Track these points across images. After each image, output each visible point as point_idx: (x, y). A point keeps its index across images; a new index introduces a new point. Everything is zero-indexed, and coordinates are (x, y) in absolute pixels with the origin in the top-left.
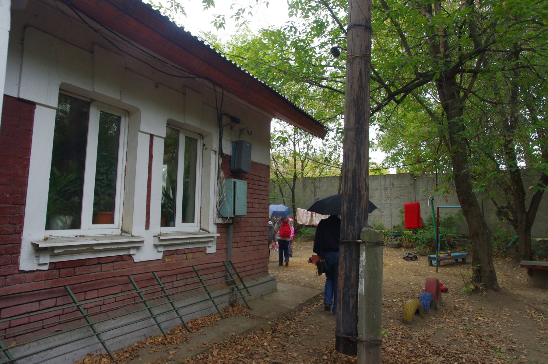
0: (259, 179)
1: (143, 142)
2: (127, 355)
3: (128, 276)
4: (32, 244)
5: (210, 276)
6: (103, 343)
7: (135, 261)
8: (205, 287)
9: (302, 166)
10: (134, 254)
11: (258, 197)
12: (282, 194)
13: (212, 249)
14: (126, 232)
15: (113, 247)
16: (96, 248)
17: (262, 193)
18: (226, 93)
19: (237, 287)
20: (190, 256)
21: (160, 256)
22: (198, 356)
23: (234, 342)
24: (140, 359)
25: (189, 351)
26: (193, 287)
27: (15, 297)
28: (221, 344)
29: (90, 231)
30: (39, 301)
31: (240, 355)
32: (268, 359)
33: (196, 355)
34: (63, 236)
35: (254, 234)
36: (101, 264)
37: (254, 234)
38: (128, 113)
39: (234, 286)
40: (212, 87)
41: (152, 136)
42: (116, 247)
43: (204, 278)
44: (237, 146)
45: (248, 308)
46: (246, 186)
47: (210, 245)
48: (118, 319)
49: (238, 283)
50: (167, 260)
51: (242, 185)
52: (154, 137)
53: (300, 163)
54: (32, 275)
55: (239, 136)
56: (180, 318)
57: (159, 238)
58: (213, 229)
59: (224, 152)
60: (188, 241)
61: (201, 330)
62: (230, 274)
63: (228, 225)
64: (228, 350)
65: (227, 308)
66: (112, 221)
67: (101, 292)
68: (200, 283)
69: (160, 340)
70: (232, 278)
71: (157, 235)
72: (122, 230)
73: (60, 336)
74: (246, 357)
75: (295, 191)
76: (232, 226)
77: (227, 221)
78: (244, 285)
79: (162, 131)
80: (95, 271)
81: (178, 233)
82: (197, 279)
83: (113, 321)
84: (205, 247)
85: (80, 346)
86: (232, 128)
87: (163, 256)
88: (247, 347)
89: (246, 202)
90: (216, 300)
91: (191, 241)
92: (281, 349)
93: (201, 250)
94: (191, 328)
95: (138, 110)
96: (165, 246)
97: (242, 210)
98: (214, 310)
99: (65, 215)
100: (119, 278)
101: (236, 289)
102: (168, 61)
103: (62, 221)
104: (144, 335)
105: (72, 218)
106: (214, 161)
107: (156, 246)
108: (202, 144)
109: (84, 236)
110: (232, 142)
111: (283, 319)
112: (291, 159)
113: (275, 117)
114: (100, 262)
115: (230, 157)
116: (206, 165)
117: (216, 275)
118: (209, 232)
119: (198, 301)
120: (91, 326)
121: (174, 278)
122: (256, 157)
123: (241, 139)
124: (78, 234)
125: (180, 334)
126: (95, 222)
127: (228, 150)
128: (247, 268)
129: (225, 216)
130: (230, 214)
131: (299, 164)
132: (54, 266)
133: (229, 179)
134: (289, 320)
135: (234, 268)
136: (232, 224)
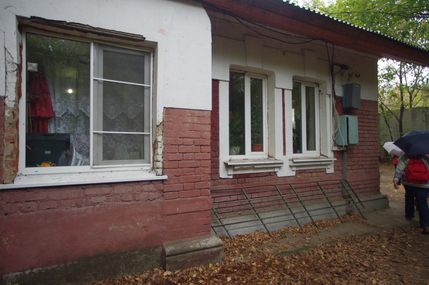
0: (368, 113)
1: (278, 94)
2: (279, 235)
3: (275, 185)
4: (224, 163)
5: (330, 190)
6: (264, 225)
7: (278, 176)
8: (327, 198)
9: (411, 97)
10: (277, 172)
11: (368, 128)
12: (388, 126)
13: (330, 170)
14: (271, 157)
15: (265, 166)
16: (256, 167)
17: (372, 125)
18: (335, 46)
19: (352, 200)
20: (314, 174)
21: (294, 174)
22: (327, 244)
23: (354, 240)
24: (287, 239)
25: (320, 240)
26: (317, 197)
27: (219, 192)
28: (343, 239)
29: (250, 156)
30: (230, 196)
31: (361, 250)
32: (387, 258)
33: (326, 244)
34: (237, 159)
35: (365, 159)
36: (259, 177)
37: (365, 159)
38: (266, 76)
39: (350, 199)
40: (325, 45)
41: (283, 90)
42: (267, 166)
43: (326, 191)
44: (348, 89)
45: (364, 218)
46: (357, 120)
47: (329, 167)
48: (271, 212)
49: (353, 197)
50: (298, 177)
51: (353, 120)
52: (285, 90)
53: (408, 95)
54: (225, 180)
55: (349, 80)
56: (311, 217)
57: (293, 161)
58: (331, 155)
59: (337, 94)
60: (312, 164)
61: (326, 228)
62: (346, 190)
63: (343, 152)
64: (350, 245)
65: (345, 215)
66: (262, 150)
67: (261, 195)
68: (323, 195)
69: (298, 230)
70: (348, 193)
71: (291, 159)
72: (268, 156)
73: (241, 217)
74: (367, 252)
75: (403, 121)
76: (346, 152)
77: (342, 149)
78: (359, 200)
79: (290, 86)
80: (256, 181)
81: (304, 158)
82: (320, 192)
83: (268, 213)
84: (325, 169)
85: (252, 225)
86: (342, 75)
87: (296, 174)
88: (366, 246)
89: (358, 133)
90: (336, 209)
91: (315, 163)
92: (399, 253)
93: (322, 170)
94: (319, 225)
95: (273, 74)
96: (297, 167)
97: (354, 139)
98: (334, 215)
99: (236, 146)
100: (269, 187)
101: (352, 202)
102: (291, 34)
103: (235, 150)
104: (287, 225)
105: (240, 148)
106: (329, 103)
107: (291, 167)
108: (318, 91)
109: (247, 159)
110: (343, 86)
111: (398, 231)
112: (398, 92)
113: (381, 57)
114: (258, 175)
115: (342, 98)
116: (322, 107)
117: (335, 190)
118: (328, 157)
119: (322, 207)
120: (257, 214)
121: (304, 190)
122: (365, 95)
123: (350, 82)
124: (245, 158)
125: (311, 228)
126: (253, 150)
127: (339, 93)
128: (361, 187)
129: (340, 145)
130: (344, 143)
131: (406, 95)
132: (236, 176)
133: (342, 116)
134: (404, 232)
135: (349, 186)
136: (346, 151)
